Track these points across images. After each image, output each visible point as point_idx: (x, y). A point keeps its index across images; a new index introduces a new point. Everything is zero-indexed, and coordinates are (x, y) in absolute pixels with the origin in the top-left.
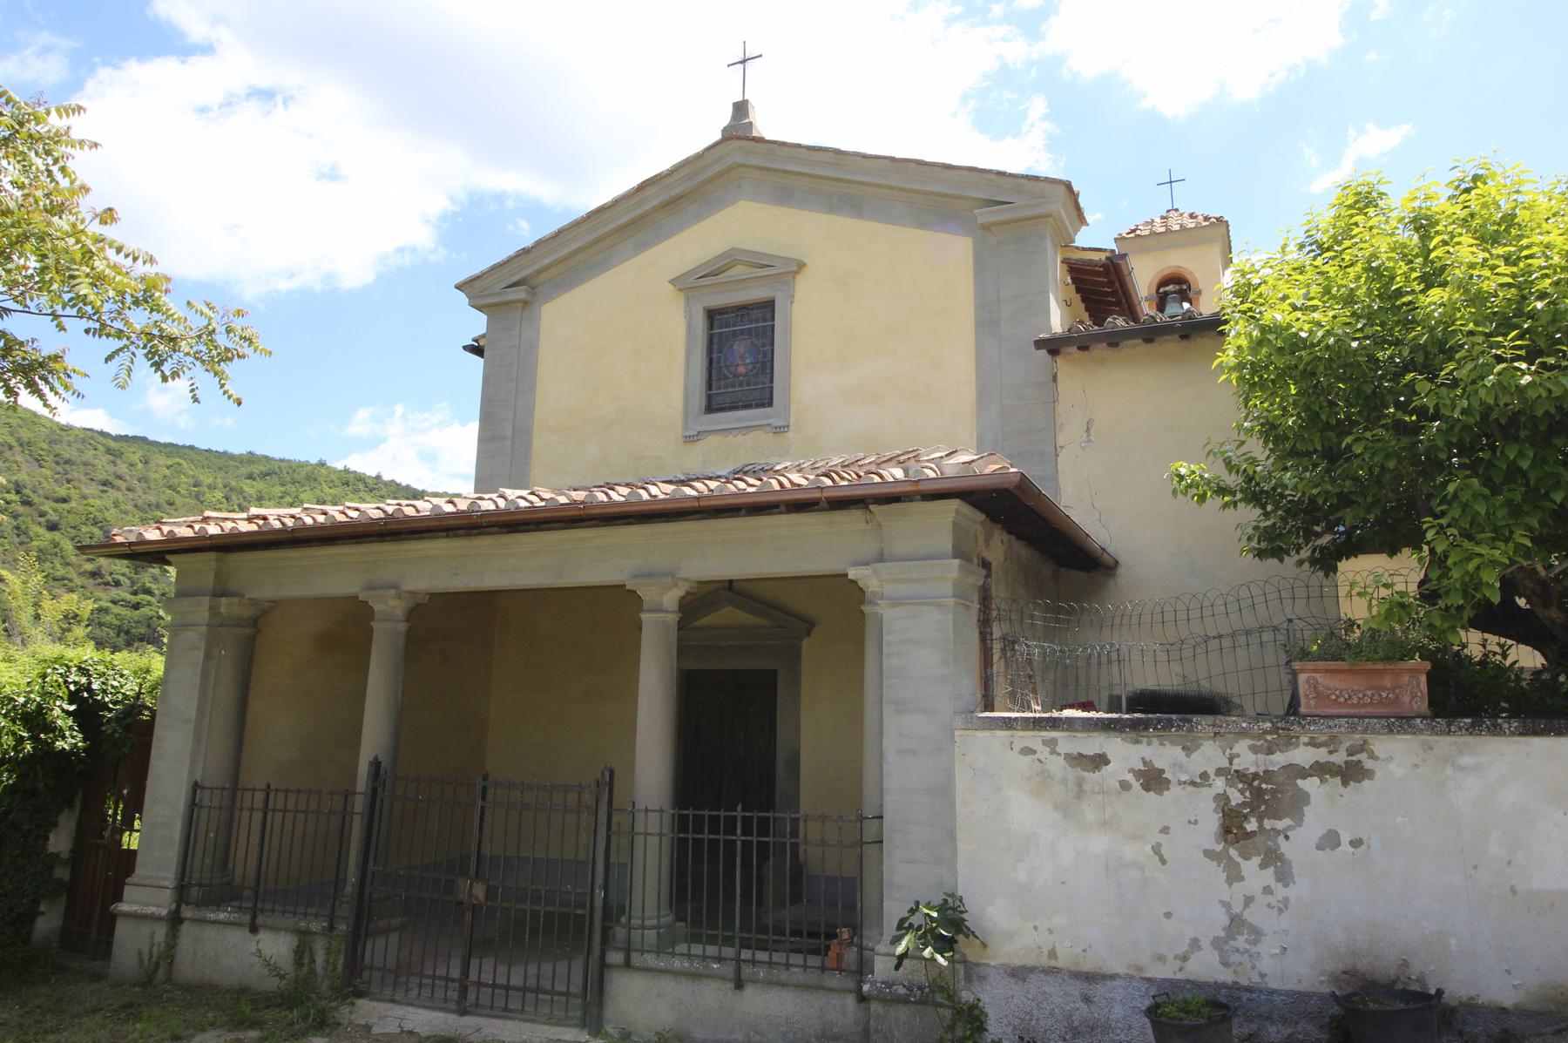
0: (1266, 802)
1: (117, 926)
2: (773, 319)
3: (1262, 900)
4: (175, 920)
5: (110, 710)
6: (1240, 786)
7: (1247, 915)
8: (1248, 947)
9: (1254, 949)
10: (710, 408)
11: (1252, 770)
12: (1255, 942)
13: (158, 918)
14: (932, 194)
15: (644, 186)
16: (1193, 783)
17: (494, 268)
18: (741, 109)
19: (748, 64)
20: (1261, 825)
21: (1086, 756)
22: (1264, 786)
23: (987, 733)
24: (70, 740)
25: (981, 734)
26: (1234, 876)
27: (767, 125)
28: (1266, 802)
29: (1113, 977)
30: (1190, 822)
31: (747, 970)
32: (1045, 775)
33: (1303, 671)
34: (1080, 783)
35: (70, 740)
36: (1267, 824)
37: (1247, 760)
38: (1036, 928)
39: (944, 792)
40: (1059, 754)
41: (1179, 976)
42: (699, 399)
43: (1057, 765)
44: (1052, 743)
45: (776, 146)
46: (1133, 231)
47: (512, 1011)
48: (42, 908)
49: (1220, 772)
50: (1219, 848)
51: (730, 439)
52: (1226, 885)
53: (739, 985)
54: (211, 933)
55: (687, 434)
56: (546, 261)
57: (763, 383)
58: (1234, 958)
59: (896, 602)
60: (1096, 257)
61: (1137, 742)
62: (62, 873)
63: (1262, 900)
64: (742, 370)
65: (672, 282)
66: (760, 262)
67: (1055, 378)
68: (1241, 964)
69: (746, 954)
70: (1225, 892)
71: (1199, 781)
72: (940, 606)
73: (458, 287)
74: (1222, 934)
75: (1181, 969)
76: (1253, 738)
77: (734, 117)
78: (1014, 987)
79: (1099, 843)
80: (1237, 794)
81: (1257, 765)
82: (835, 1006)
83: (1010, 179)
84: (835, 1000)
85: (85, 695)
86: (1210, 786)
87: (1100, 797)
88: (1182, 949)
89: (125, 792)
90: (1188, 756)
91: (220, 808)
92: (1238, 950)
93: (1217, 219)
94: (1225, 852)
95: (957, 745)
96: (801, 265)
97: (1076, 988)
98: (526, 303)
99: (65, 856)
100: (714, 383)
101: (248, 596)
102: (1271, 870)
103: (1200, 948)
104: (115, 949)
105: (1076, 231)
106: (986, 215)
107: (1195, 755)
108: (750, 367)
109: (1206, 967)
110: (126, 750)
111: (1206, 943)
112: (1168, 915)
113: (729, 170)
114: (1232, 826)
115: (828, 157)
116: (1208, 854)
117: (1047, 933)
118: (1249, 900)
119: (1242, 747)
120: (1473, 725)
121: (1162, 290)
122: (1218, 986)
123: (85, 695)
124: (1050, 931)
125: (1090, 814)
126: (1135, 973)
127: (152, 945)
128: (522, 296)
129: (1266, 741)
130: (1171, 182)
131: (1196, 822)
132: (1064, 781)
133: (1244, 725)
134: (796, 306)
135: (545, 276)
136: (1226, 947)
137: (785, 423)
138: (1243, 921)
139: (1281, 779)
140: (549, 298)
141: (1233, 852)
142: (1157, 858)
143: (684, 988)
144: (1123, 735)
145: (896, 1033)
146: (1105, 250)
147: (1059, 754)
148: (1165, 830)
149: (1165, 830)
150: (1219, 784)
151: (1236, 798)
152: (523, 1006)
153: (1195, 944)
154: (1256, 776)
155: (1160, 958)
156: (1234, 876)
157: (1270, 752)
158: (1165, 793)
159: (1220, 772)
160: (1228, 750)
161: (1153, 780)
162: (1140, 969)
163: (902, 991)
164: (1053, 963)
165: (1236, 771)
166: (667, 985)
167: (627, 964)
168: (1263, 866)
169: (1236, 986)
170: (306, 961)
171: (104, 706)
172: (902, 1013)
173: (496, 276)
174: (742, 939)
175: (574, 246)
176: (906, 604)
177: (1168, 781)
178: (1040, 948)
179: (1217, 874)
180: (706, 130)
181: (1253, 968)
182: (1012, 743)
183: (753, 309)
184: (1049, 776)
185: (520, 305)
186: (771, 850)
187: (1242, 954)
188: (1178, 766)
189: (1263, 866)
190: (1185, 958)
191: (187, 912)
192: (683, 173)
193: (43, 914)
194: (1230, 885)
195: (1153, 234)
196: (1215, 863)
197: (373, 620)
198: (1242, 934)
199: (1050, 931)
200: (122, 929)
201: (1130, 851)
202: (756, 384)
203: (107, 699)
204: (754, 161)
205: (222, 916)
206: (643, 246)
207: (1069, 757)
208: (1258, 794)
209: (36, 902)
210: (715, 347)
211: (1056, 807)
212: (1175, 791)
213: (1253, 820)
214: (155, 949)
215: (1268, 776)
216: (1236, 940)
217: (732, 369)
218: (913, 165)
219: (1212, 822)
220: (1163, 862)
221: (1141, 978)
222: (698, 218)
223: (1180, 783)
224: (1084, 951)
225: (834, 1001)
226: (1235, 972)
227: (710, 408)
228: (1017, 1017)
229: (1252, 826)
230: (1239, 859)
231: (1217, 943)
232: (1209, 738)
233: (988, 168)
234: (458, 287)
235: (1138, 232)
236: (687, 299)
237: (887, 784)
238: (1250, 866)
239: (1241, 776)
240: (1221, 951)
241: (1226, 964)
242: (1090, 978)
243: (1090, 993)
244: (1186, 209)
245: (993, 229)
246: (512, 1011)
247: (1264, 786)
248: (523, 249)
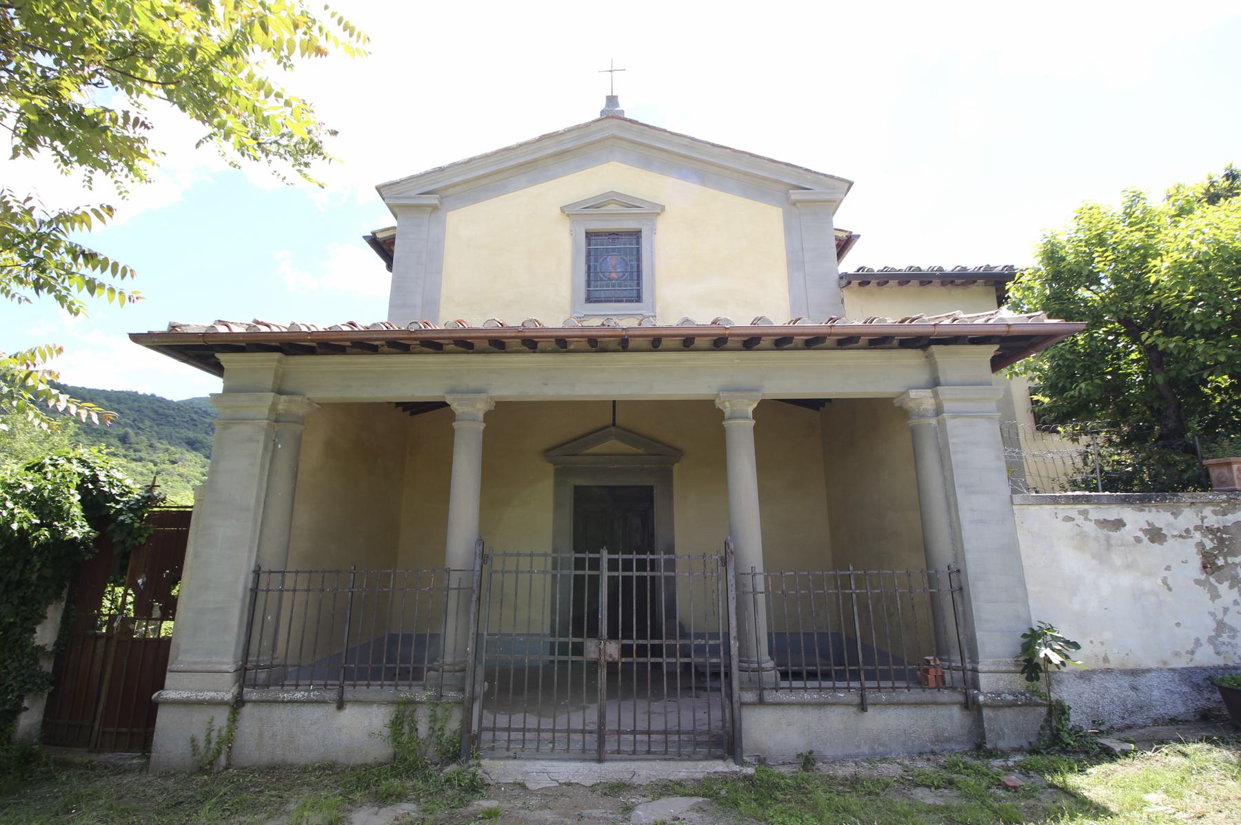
0: (1227, 546)
1: (158, 713)
3: (1233, 609)
4: (238, 703)
5: (118, 502)
6: (1210, 536)
7: (1227, 620)
8: (1230, 640)
9: (1233, 642)
10: (589, 300)
11: (1216, 526)
12: (1233, 637)
13: (222, 703)
14: (756, 176)
15: (542, 138)
16: (1181, 536)
17: (411, 178)
18: (612, 100)
20: (1226, 562)
21: (1108, 521)
22: (1224, 536)
23: (1037, 507)
24: (79, 530)
25: (1032, 508)
26: (1215, 595)
28: (1227, 546)
29: (1149, 671)
30: (1183, 562)
31: (870, 696)
32: (1083, 535)
33: (1236, 463)
34: (1108, 539)
35: (79, 530)
36: (1230, 560)
37: (1213, 520)
38: (1091, 642)
39: (1012, 549)
40: (1091, 520)
41: (1191, 665)
42: (582, 295)
43: (1090, 527)
44: (1084, 513)
45: (647, 128)
47: (655, 753)
48: (26, 704)
49: (1197, 528)
50: (1203, 577)
52: (1211, 602)
53: (863, 707)
54: (281, 712)
56: (456, 180)
57: (631, 286)
58: (1223, 649)
59: (957, 415)
61: (1142, 510)
62: (47, 666)
63: (1233, 609)
64: (614, 275)
66: (630, 204)
68: (1227, 652)
69: (868, 684)
70: (1212, 606)
71: (1185, 534)
72: (989, 418)
74: (1213, 634)
75: (1191, 660)
76: (1213, 506)
77: (607, 105)
78: (1084, 685)
79: (1126, 580)
80: (1209, 542)
81: (1219, 523)
82: (943, 716)
83: (814, 175)
84: (943, 711)
85: (91, 486)
86: (1192, 537)
87: (1123, 548)
88: (1190, 646)
89: (140, 581)
90: (1176, 518)
91: (308, 590)
92: (1224, 643)
94: (1207, 580)
95: (1016, 515)
97: (1125, 681)
98: (435, 208)
99: (49, 649)
100: (592, 283)
101: (308, 396)
102: (1236, 589)
103: (1201, 645)
104: (158, 738)
106: (795, 195)
107: (1179, 517)
108: (621, 274)
109: (1206, 657)
110: (143, 541)
111: (1204, 641)
112: (1178, 624)
113: (607, 138)
114: (1209, 564)
115: (686, 142)
116: (1197, 582)
117: (1100, 645)
118: (1226, 610)
119: (1208, 511)
120: (1228, 501)
122: (1216, 669)
123: (91, 486)
124: (1102, 644)
125: (1117, 560)
126: (1162, 666)
127: (210, 730)
129: (1222, 507)
131: (1186, 562)
132: (1096, 539)
133: (1211, 497)
135: (451, 191)
136: (1217, 642)
138: (1225, 624)
139: (1234, 531)
141: (1212, 580)
142: (1166, 587)
143: (812, 715)
144: (1133, 506)
145: (1006, 730)
146: (846, 231)
147: (1091, 520)
148: (1168, 568)
149: (1168, 568)
150: (1197, 536)
151: (1209, 545)
152: (667, 748)
153: (1198, 642)
154: (1218, 529)
155: (1177, 654)
156: (1215, 595)
157: (1225, 514)
158: (1165, 543)
159: (1197, 528)
160: (1200, 515)
161: (1156, 535)
162: (1165, 663)
163: (1010, 698)
164: (1107, 666)
165: (1207, 527)
166: (795, 714)
167: (761, 702)
168: (1231, 587)
169: (1226, 668)
170: (406, 729)
171: (111, 498)
172: (1009, 714)
173: (414, 184)
174: (866, 672)
175: (481, 172)
176: (964, 416)
177: (1165, 536)
178: (1096, 656)
179: (1203, 594)
180: (591, 111)
181: (1235, 653)
182: (1056, 513)
183: (621, 235)
184: (1085, 536)
185: (430, 209)
186: (571, 603)
187: (1227, 645)
188: (1170, 525)
189: (1231, 587)
190: (1192, 653)
191: (252, 694)
192: (575, 134)
193: (26, 709)
194: (1213, 601)
196: (1202, 588)
197: (454, 421)
198: (1224, 632)
199: (1102, 644)
200: (164, 718)
201: (1147, 584)
203: (114, 492)
204: (629, 136)
205: (299, 695)
206: (535, 182)
207: (1098, 522)
208: (1221, 541)
209: (21, 698)
210: (592, 258)
211: (1093, 557)
212: (1170, 542)
213: (1221, 558)
214: (214, 735)
215: (1226, 529)
216: (1222, 636)
217: (607, 274)
218: (748, 156)
219: (1197, 561)
220: (1170, 589)
221: (1168, 669)
222: (579, 168)
223: (1174, 536)
224: (1127, 654)
225: (943, 712)
226: (1225, 658)
227: (589, 300)
228: (1089, 707)
229: (1220, 562)
230: (1216, 584)
231: (1211, 640)
232: (1187, 506)
233: (800, 165)
237: (967, 546)
238: (1223, 588)
239: (1210, 530)
240: (1214, 644)
241: (1218, 653)
242: (1134, 673)
243: (1135, 683)
245: (798, 204)
246: (655, 753)
247: (1224, 536)
248: (440, 168)
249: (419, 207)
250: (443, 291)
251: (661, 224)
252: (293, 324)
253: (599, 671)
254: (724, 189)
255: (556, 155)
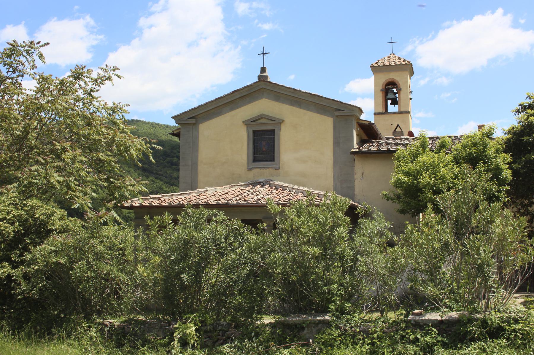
2: (274, 135)
15: (234, 92)
18: (263, 70)
19: (262, 52)
27: (273, 77)
42: (251, 158)
46: (377, 63)
51: (262, 170)
55: (249, 168)
56: (201, 112)
60: (366, 123)
64: (264, 149)
65: (243, 122)
66: (271, 119)
67: (354, 160)
73: (173, 118)
93: (408, 62)
96: (283, 121)
105: (360, 115)
106: (337, 113)
115: (292, 91)
121: (387, 87)
128: (194, 122)
130: (392, 42)
134: (281, 133)
137: (278, 167)
140: (202, 122)
180: (252, 79)
192: (247, 89)
195: (384, 65)
202: (269, 154)
204: (269, 88)
206: (232, 109)
222: (250, 102)
234: (173, 118)
235: (379, 64)
236: (247, 127)
244: (398, 55)
249: (189, 124)
250: (199, 159)
251: (283, 127)
252: (381, 90)
253: (227, 186)
254: (309, 110)
255: (240, 98)
